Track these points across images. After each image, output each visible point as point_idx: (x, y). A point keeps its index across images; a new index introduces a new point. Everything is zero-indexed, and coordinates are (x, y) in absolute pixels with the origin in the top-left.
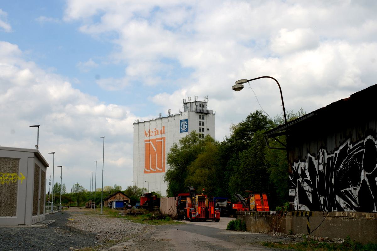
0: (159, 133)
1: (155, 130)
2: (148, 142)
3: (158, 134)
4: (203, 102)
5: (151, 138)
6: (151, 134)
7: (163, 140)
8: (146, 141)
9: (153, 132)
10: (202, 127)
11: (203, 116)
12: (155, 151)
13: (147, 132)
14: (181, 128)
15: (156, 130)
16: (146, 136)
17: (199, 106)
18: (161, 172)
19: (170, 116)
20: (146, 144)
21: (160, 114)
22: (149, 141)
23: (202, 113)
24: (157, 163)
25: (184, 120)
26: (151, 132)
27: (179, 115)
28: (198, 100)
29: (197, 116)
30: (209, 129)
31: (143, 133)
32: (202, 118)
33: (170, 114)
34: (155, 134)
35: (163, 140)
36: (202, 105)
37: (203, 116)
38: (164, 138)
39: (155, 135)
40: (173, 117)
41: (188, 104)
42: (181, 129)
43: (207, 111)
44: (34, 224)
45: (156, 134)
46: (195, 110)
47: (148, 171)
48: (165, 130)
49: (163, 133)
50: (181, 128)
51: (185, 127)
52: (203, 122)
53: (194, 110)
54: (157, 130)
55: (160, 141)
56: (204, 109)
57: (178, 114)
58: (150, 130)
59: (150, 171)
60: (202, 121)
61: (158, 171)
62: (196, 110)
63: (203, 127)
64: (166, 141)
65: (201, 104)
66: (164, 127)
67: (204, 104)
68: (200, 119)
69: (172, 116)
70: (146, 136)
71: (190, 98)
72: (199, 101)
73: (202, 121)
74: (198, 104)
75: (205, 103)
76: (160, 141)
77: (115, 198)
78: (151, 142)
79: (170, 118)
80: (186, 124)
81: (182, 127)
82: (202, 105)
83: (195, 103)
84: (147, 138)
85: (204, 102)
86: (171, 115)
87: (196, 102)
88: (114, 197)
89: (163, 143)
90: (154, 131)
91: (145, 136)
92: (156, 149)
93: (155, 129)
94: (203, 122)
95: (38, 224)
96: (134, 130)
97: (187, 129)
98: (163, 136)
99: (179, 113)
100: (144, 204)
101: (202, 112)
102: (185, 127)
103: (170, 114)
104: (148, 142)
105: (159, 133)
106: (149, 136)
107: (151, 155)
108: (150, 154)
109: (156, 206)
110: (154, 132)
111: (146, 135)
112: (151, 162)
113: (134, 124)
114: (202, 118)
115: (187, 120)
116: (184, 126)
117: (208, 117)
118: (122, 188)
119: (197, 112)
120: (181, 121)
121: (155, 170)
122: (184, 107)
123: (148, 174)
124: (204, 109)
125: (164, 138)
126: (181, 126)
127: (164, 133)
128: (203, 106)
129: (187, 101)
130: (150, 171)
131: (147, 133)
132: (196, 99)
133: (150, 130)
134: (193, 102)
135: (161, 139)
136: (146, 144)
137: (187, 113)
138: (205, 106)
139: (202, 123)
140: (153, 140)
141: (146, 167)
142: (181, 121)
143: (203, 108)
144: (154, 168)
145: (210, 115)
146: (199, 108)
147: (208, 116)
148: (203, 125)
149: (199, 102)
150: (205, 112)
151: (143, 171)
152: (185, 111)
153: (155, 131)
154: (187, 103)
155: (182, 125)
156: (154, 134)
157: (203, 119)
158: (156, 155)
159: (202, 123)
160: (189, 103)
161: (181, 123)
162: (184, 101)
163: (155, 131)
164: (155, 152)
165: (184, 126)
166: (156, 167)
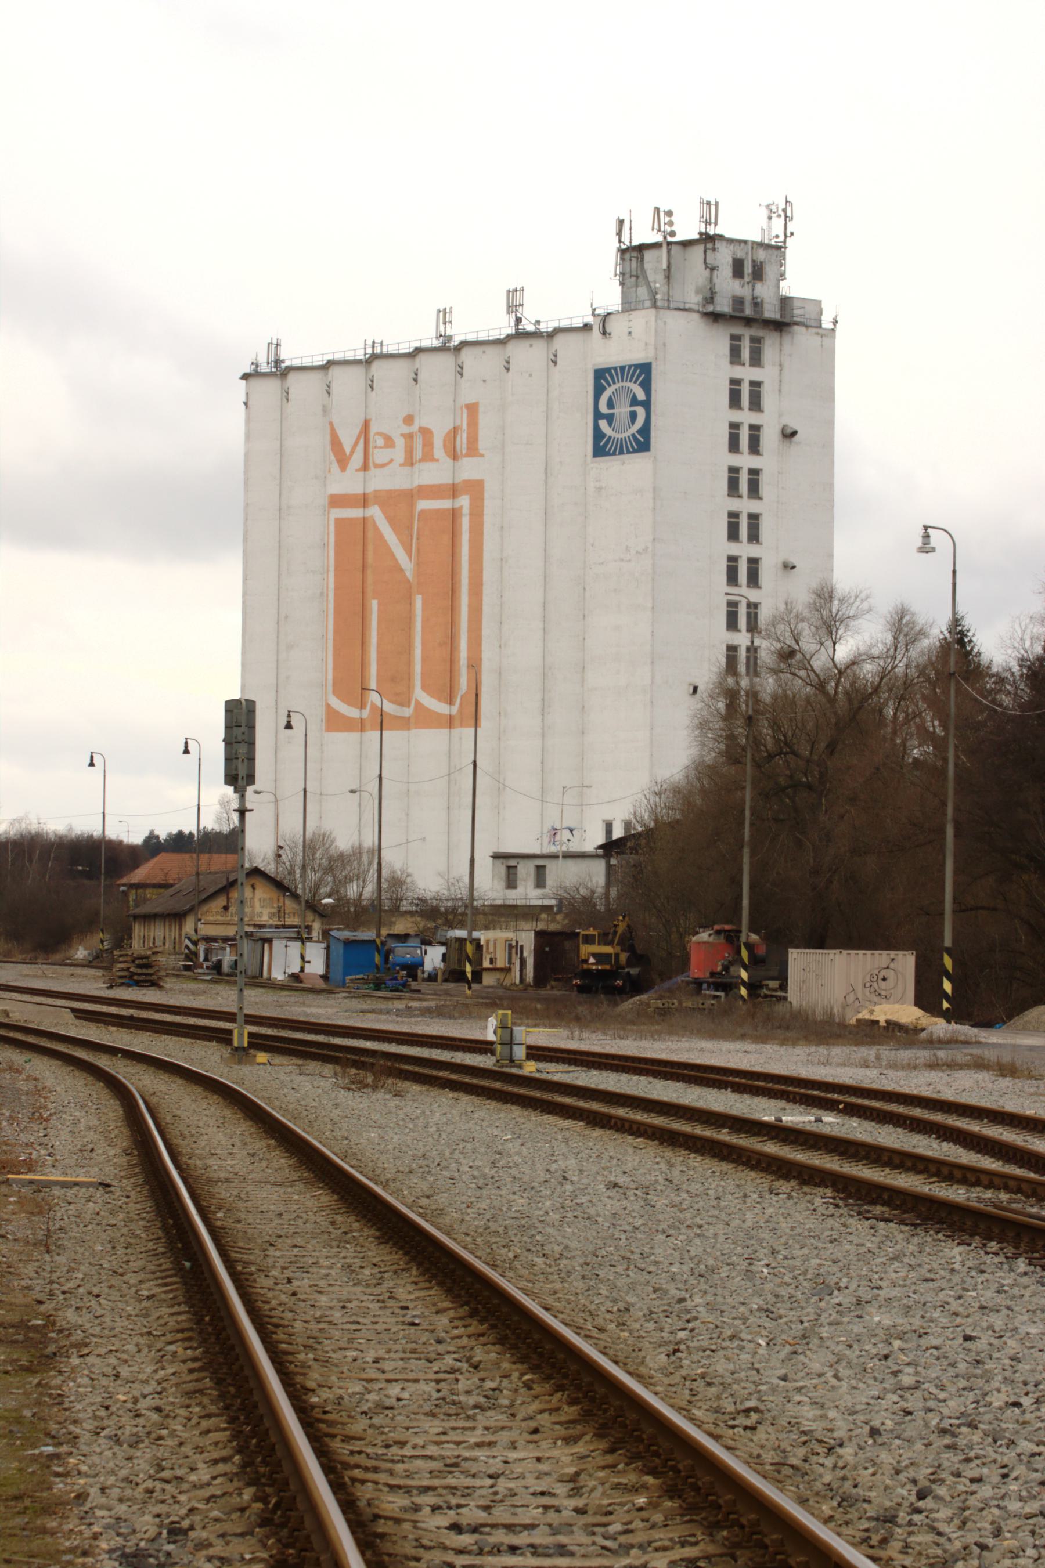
0: (439, 451)
1: (406, 430)
2: (356, 513)
3: (428, 457)
4: (753, 243)
5: (379, 481)
6: (379, 455)
7: (464, 502)
8: (337, 501)
9: (389, 442)
10: (746, 417)
11: (756, 341)
12: (409, 574)
13: (347, 441)
14: (603, 424)
15: (415, 428)
16: (343, 467)
17: (726, 271)
18: (450, 722)
19: (521, 335)
20: (339, 522)
21: (444, 315)
22: (364, 501)
23: (748, 322)
24: (424, 660)
25: (622, 371)
26: (380, 442)
27: (587, 327)
28: (725, 228)
29: (719, 340)
30: (794, 433)
31: (320, 441)
32: (746, 354)
33: (518, 321)
34: (409, 452)
35: (464, 502)
36: (748, 269)
37: (756, 341)
38: (475, 489)
39: (410, 461)
40: (539, 345)
41: (648, 255)
42: (598, 434)
43: (785, 302)
44: (966, 1043)
45: (418, 454)
46: (699, 298)
47: (353, 712)
48: (483, 433)
49: (467, 455)
50: (603, 424)
51: (633, 416)
52: (756, 385)
53: (693, 299)
54: (426, 432)
55: (446, 504)
56: (763, 290)
57: (578, 323)
58: (366, 424)
59: (366, 713)
60: (747, 373)
61: (425, 719)
62: (710, 299)
63: (754, 418)
64: (490, 506)
65: (740, 254)
66: (472, 409)
67: (761, 255)
68: (732, 363)
69: (536, 335)
70: (343, 467)
71: (669, 213)
72: (728, 235)
73: (747, 373)
74: (724, 257)
75: (768, 246)
76: (446, 504)
77: (226, 908)
78: (375, 512)
79: (519, 351)
80: (641, 396)
81: (610, 419)
82: (748, 269)
83: (699, 250)
84: (349, 483)
85: (761, 245)
86: (530, 328)
87: (708, 240)
88: (221, 901)
89: (465, 523)
90: (397, 430)
91: (335, 467)
92: (418, 564)
93: (409, 420)
94: (756, 385)
95: (962, 1038)
96: (248, 420)
97: (646, 430)
98: (469, 470)
99: (590, 319)
100: (713, 974)
101: (748, 311)
102: (633, 416)
103: (518, 321)
104: (356, 513)
105: (439, 451)
106: (365, 467)
107: (374, 604)
108: (370, 589)
109: (774, 984)
110: (400, 442)
111: (343, 462)
112: (379, 652)
113: (245, 377)
114: (746, 354)
115: (643, 372)
116: (622, 411)
117: (787, 347)
118: (156, 833)
119: (715, 317)
120: (602, 377)
121: (407, 712)
122: (623, 274)
123: (355, 736)
124: (763, 290)
125: (475, 489)
126: (603, 409)
127: (473, 450)
128: (758, 273)
129: (644, 234)
130: (366, 713)
131: (348, 451)
132: (708, 223)
133: (366, 424)
134: (686, 244)
135: (453, 491)
136: (339, 522)
137: (642, 320)
138: (770, 272)
139: (745, 390)
140: (389, 500)
141: (340, 689)
142: (602, 377)
143: (758, 286)
144: (403, 700)
145: (801, 337)
146: (728, 287)
147: (787, 339)
148: (756, 404)
149: (731, 241)
150: (771, 312)
151: (321, 712)
152: (629, 305)
153: (409, 437)
154: (642, 248)
155: (610, 404)
156: (398, 453)
157: (756, 360)
158: (411, 604)
159: (745, 390)
160: (656, 245)
161: (599, 391)
162: (619, 234)
163: (409, 437)
164: (408, 581)
165: (622, 411)
166: (410, 688)
